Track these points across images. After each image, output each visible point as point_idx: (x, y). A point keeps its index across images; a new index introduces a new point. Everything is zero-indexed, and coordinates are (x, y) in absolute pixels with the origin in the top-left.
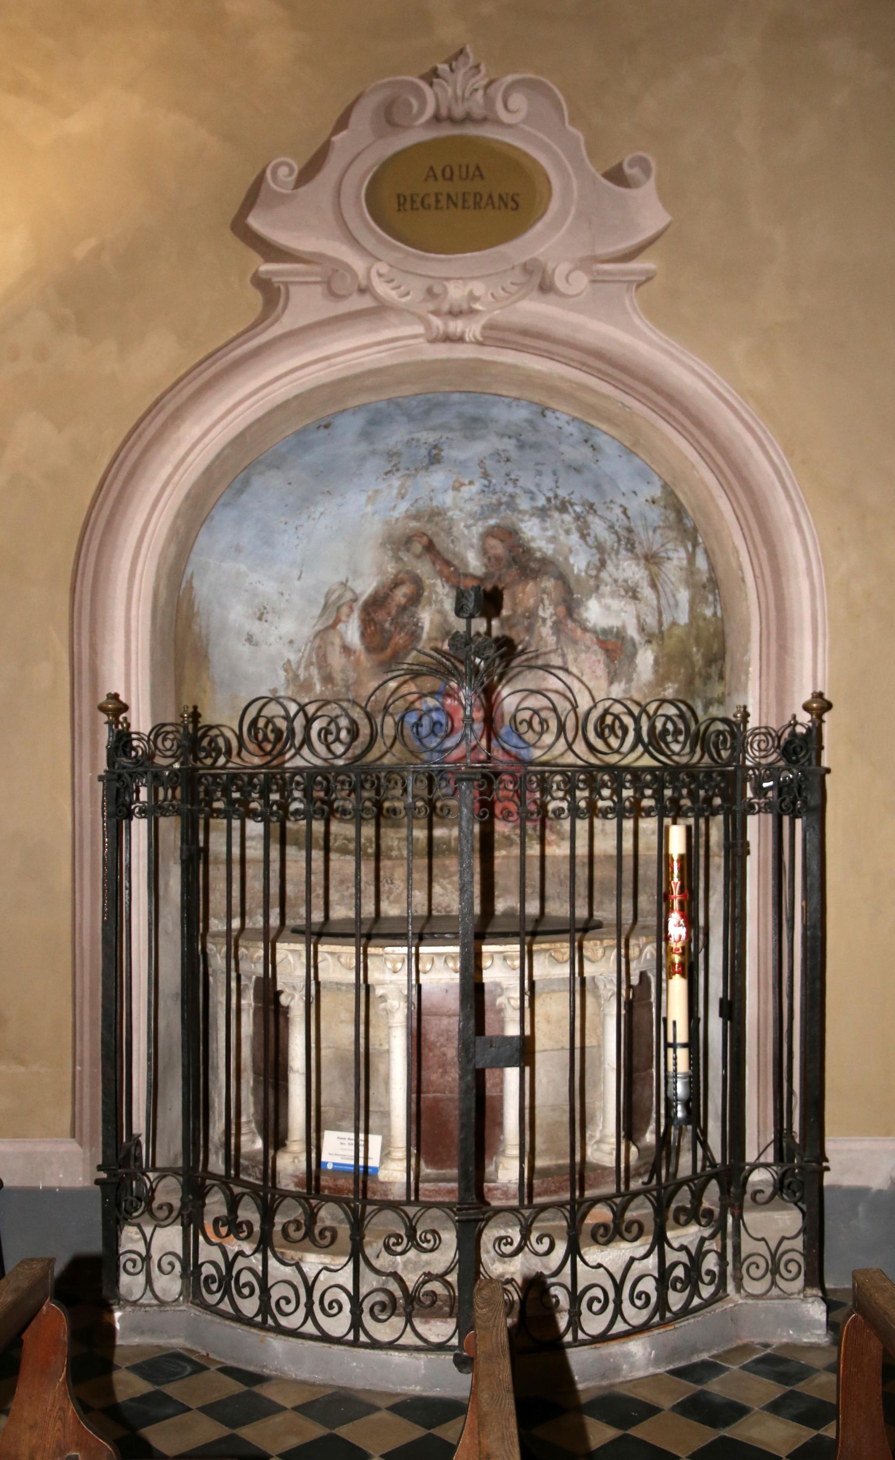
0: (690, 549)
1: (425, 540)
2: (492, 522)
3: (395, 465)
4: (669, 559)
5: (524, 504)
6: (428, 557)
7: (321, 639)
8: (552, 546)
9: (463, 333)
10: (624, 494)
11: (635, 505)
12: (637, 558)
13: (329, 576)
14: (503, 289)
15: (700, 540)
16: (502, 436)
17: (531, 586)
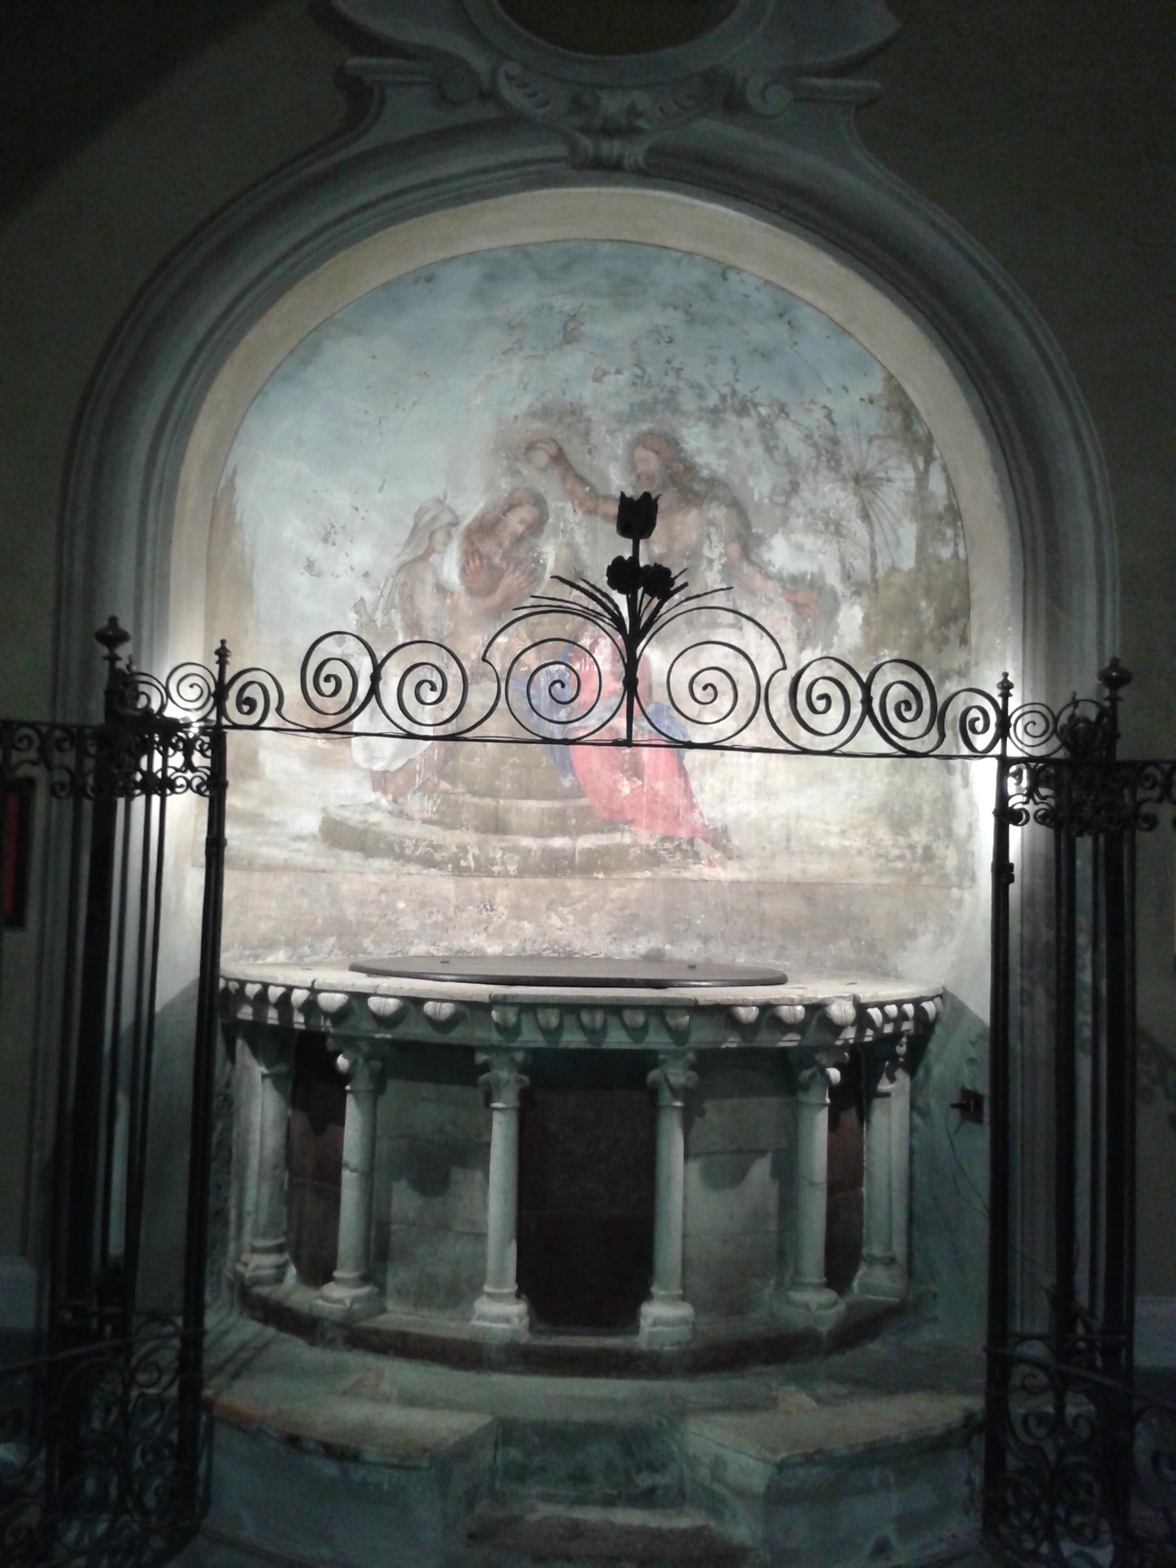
0: (921, 465)
1: (553, 450)
2: (645, 427)
3: (518, 341)
4: (889, 480)
5: (688, 402)
6: (555, 473)
8: (724, 462)
9: (621, 157)
10: (829, 391)
11: (843, 406)
12: (844, 479)
13: (424, 492)
15: (936, 453)
16: (665, 305)
17: (693, 515)
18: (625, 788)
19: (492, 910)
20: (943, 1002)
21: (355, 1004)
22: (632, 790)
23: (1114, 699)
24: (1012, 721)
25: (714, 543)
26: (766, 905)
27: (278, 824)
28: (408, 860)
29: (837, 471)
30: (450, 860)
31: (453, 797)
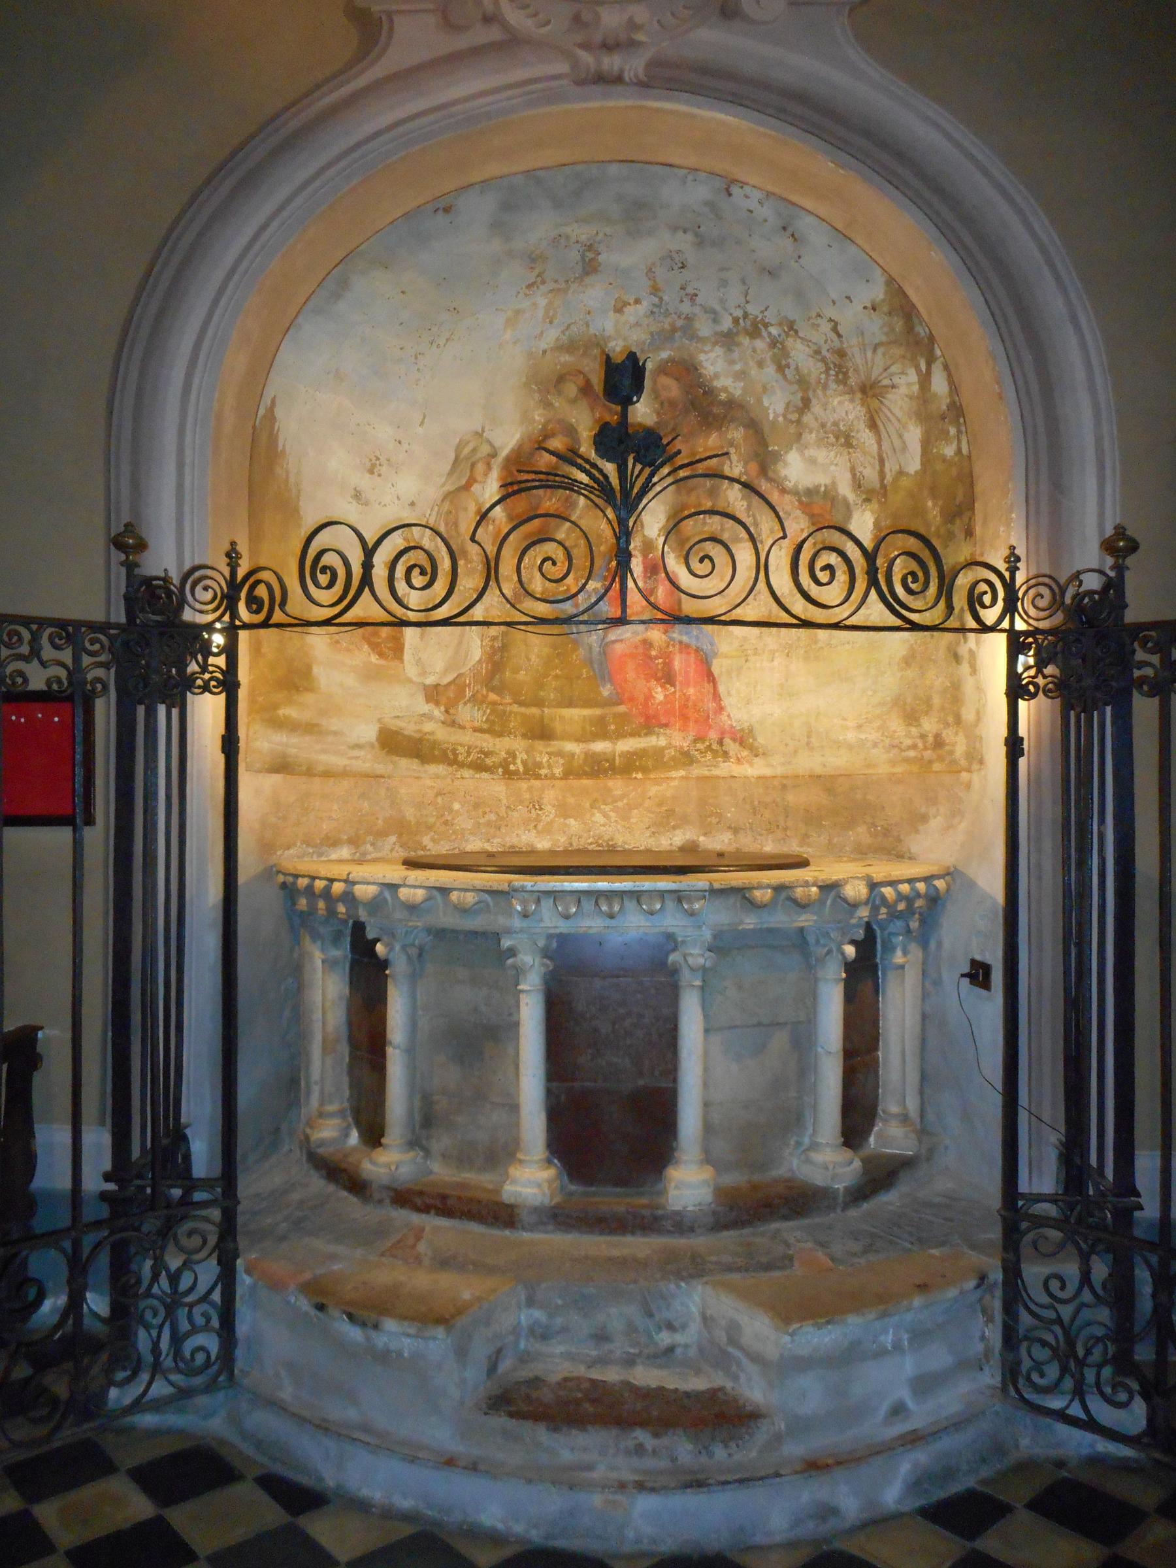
0: (923, 367)
1: (581, 381)
5: (704, 328)
7: (451, 502)
9: (622, 71)
10: (834, 302)
11: (850, 316)
12: (851, 392)
13: (463, 424)
14: (673, 14)
15: (938, 352)
16: (675, 229)
18: (659, 695)
19: (541, 809)
20: (954, 880)
21: (387, 895)
22: (666, 696)
23: (1120, 569)
24: (1020, 594)
25: (735, 463)
26: (791, 798)
27: (335, 733)
28: (462, 765)
29: (845, 384)
30: (500, 765)
31: (501, 707)
